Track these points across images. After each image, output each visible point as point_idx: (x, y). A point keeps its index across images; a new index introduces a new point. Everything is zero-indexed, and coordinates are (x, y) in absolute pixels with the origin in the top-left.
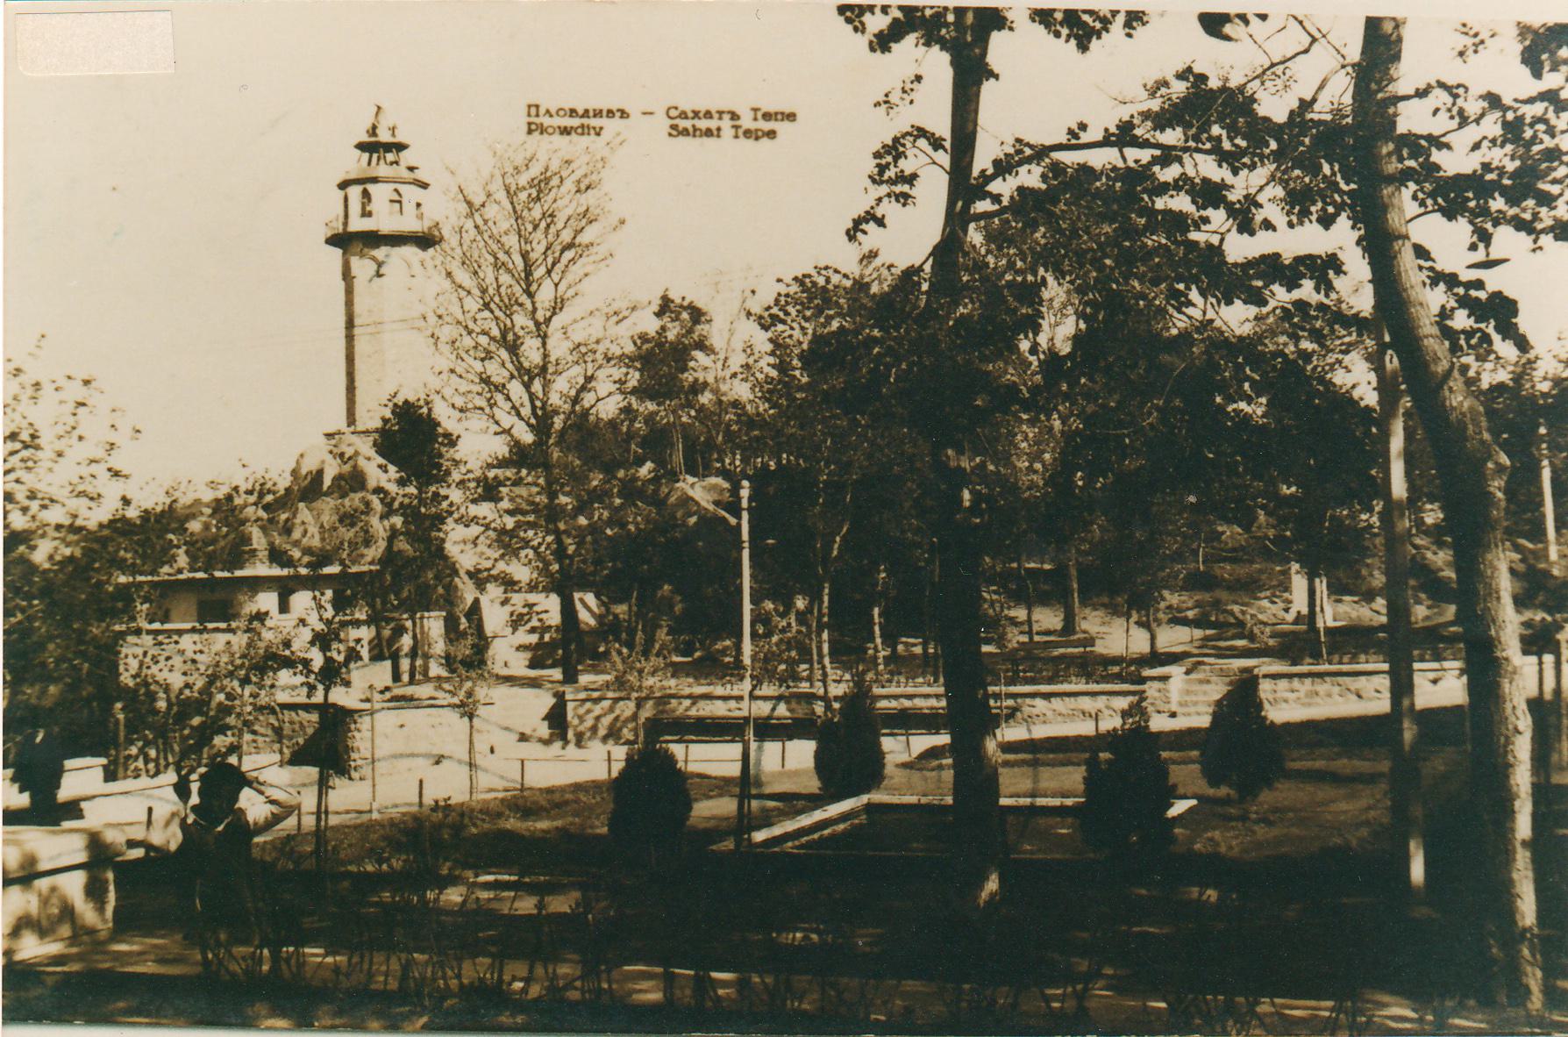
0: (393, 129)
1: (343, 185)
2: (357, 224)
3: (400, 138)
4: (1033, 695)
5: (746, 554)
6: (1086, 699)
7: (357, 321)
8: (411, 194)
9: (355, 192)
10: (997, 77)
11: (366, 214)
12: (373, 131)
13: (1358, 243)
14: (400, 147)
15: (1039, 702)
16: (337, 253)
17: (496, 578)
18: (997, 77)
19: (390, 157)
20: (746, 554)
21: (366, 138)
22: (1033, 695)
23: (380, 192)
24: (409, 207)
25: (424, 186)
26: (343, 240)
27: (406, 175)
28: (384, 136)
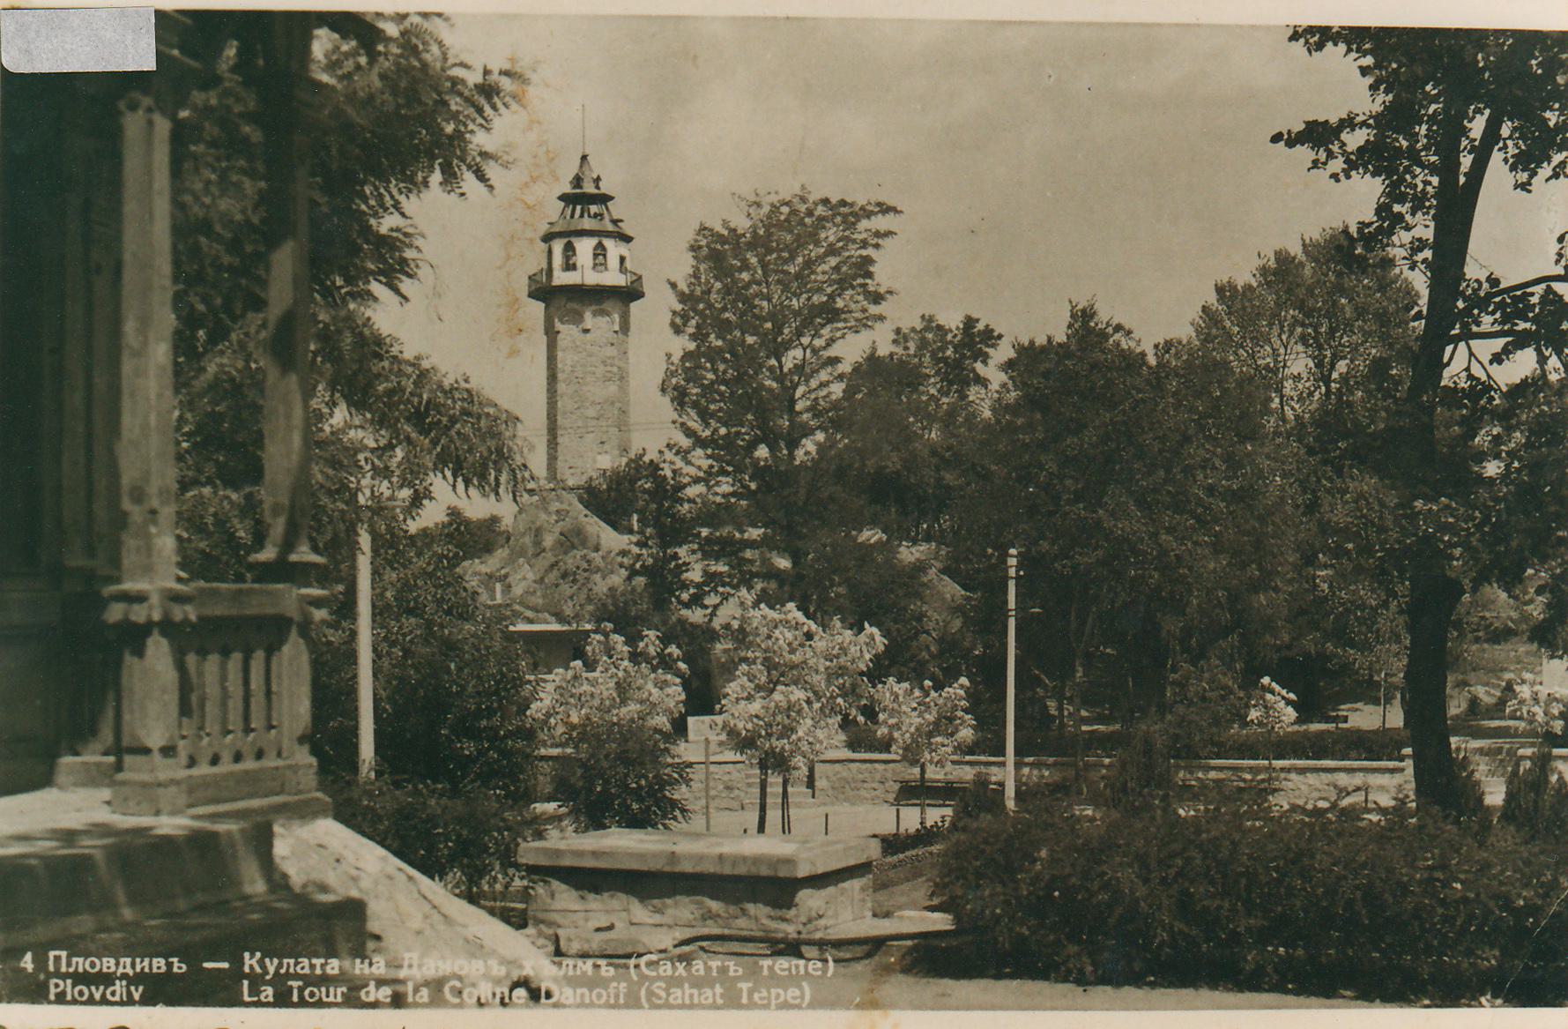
0: (598, 180)
1: (548, 238)
2: (561, 278)
3: (605, 188)
4: (1289, 770)
5: (1012, 623)
6: (1342, 775)
7: (560, 376)
8: (614, 249)
9: (558, 247)
10: (612, 198)
11: (569, 266)
12: (577, 181)
13: (928, 320)
14: (604, 199)
15: (1293, 776)
16: (538, 308)
17: (258, 522)
18: (612, 198)
19: (594, 209)
20: (1012, 623)
21: (568, 189)
22: (1289, 770)
23: (584, 247)
24: (613, 262)
25: (627, 239)
26: (544, 291)
27: (610, 227)
28: (589, 188)
